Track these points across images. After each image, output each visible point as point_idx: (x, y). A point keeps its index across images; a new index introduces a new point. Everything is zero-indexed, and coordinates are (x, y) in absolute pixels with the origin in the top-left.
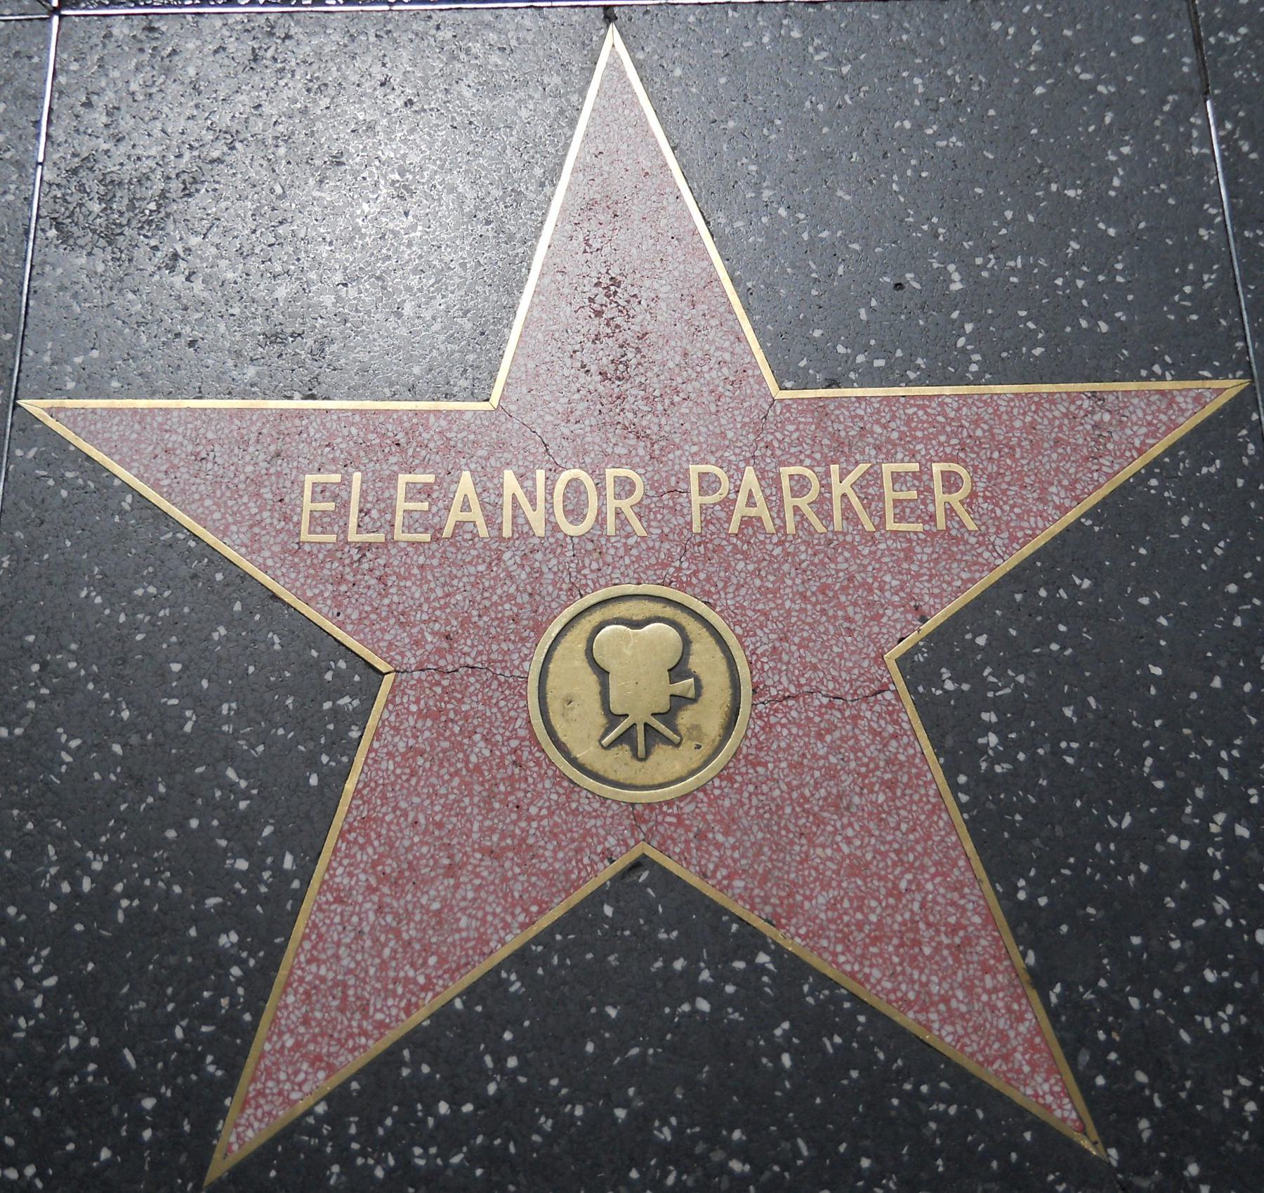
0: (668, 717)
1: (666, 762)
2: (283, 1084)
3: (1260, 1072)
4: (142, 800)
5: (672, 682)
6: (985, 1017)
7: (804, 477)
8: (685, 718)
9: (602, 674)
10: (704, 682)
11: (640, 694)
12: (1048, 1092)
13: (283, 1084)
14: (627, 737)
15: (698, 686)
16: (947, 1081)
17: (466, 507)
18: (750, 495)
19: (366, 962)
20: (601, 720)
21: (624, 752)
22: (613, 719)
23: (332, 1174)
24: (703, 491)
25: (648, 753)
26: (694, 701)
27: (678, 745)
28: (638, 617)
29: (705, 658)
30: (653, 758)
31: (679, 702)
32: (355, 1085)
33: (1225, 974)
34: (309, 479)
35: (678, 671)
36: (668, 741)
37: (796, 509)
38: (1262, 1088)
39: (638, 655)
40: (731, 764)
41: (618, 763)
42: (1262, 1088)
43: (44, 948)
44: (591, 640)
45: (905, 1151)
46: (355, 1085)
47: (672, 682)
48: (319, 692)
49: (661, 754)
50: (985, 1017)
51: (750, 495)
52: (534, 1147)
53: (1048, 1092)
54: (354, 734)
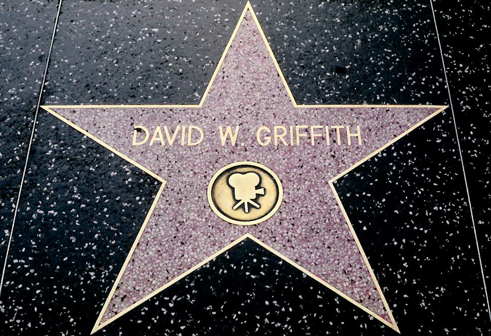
0: (255, 200)
1: (255, 213)
8: (261, 200)
11: (246, 194)
18: (158, 133)
20: (232, 202)
21: (241, 210)
25: (249, 211)
26: (263, 195)
29: (267, 183)
32: (281, 263)
33: (14, 304)
35: (258, 187)
38: (180, 335)
40: (150, 221)
42: (180, 335)
45: (222, 308)
46: (281, 263)
47: (256, 189)
51: (158, 133)
54: (19, 210)
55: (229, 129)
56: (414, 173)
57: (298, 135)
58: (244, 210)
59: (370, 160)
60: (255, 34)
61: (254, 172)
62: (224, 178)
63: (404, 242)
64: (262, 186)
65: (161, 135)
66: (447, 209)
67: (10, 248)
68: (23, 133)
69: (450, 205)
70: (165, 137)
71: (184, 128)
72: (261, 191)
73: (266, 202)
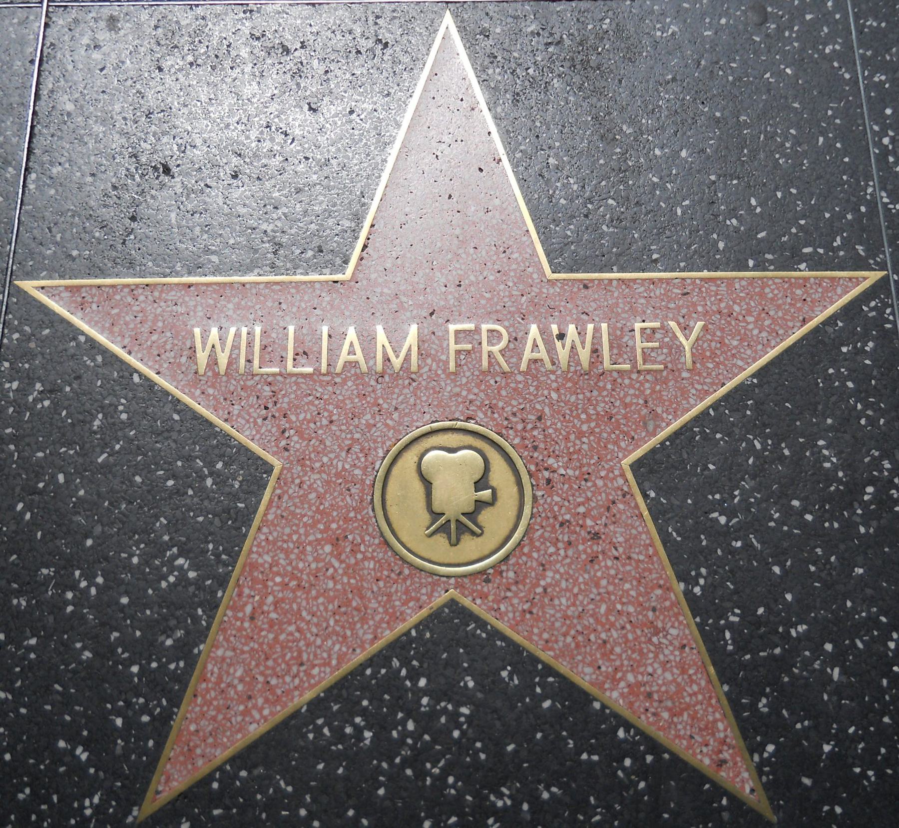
0: (472, 515)
1: (470, 546)
2: (227, 709)
4: (336, 745)
6: (700, 729)
7: (498, 331)
8: (485, 517)
9: (427, 484)
10: (499, 495)
11: (454, 494)
12: (743, 780)
13: (227, 709)
14: (444, 529)
16: (535, 691)
17: (352, 352)
20: (426, 517)
22: (436, 515)
24: (490, 343)
25: (480, 527)
28: (454, 445)
29: (500, 475)
31: (480, 505)
34: (452, 328)
35: (481, 484)
37: (490, 355)
39: (453, 468)
41: (439, 547)
44: (421, 459)
50: (700, 729)
53: (743, 780)
59: (322, 695)
61: (470, 447)
63: (810, 566)
64: (487, 482)
67: (878, 212)
68: (677, 148)
69: (599, 810)
71: (244, 331)
73: (496, 521)
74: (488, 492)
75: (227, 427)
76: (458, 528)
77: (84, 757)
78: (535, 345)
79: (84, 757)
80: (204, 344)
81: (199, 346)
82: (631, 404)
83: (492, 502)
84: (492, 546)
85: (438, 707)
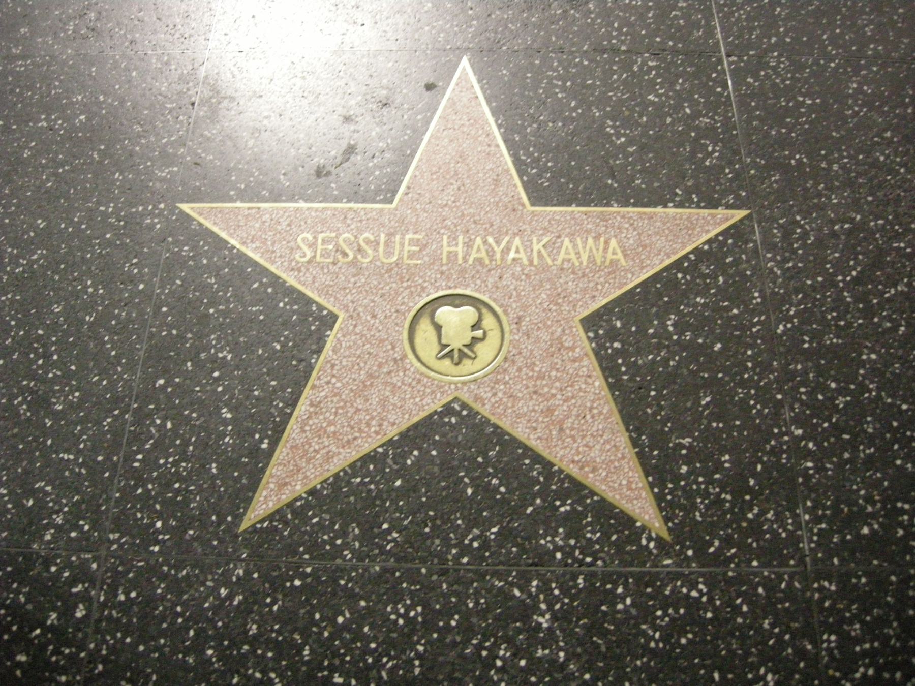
0: (469, 346)
3: (200, 684)
5: (472, 331)
8: (479, 347)
11: (457, 336)
14: (450, 355)
15: (485, 333)
19: (325, 437)
20: (436, 347)
23: (889, 292)
27: (475, 358)
29: (489, 322)
30: (479, 354)
35: (475, 327)
36: (470, 357)
43: (256, 288)
48: (308, 326)
49: (467, 362)
52: (729, 469)
55: (590, 241)
56: (659, 358)
57: (407, 248)
58: (452, 358)
60: (472, 121)
62: (429, 309)
65: (619, 251)
66: (366, 640)
70: (578, 253)
72: (479, 333)
73: (486, 351)
74: (481, 332)
75: (569, 209)
76: (459, 356)
77: (835, 540)
78: (479, 250)
79: (835, 540)
80: (584, 248)
81: (582, 252)
82: (623, 454)
83: (482, 339)
84: (479, 368)
85: (112, 205)
